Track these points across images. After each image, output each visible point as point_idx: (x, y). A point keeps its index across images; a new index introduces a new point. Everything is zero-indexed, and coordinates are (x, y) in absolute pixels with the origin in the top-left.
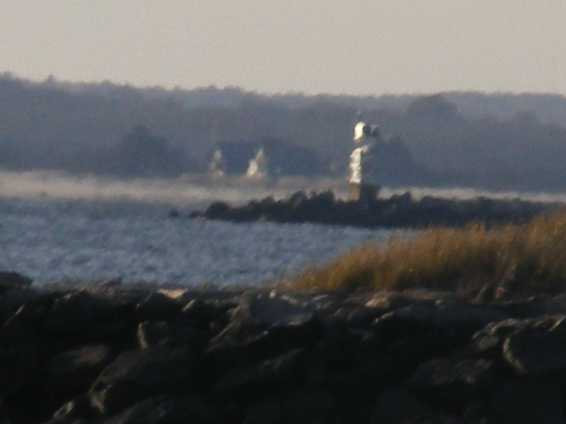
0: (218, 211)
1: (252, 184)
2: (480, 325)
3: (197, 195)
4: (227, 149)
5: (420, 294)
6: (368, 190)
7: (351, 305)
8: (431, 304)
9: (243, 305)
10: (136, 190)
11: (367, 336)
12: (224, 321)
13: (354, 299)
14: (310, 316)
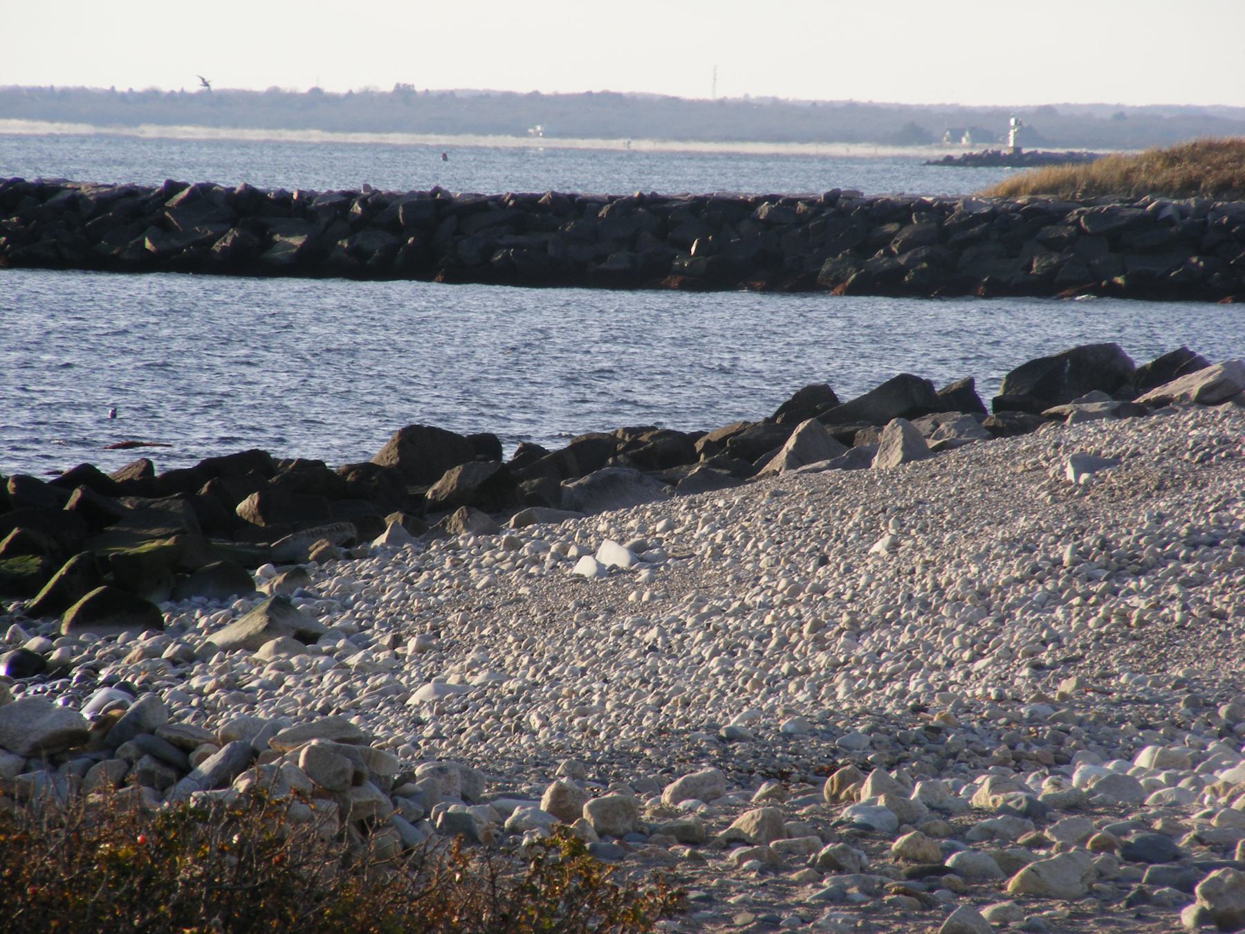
0: (949, 161)
1: (965, 147)
2: (1070, 210)
3: (938, 153)
4: (952, 131)
5: (1043, 197)
6: (1017, 150)
7: (1011, 203)
8: (1047, 201)
9: (960, 204)
10: (909, 151)
11: (1018, 216)
12: (952, 211)
13: (1012, 199)
14: (990, 208)
